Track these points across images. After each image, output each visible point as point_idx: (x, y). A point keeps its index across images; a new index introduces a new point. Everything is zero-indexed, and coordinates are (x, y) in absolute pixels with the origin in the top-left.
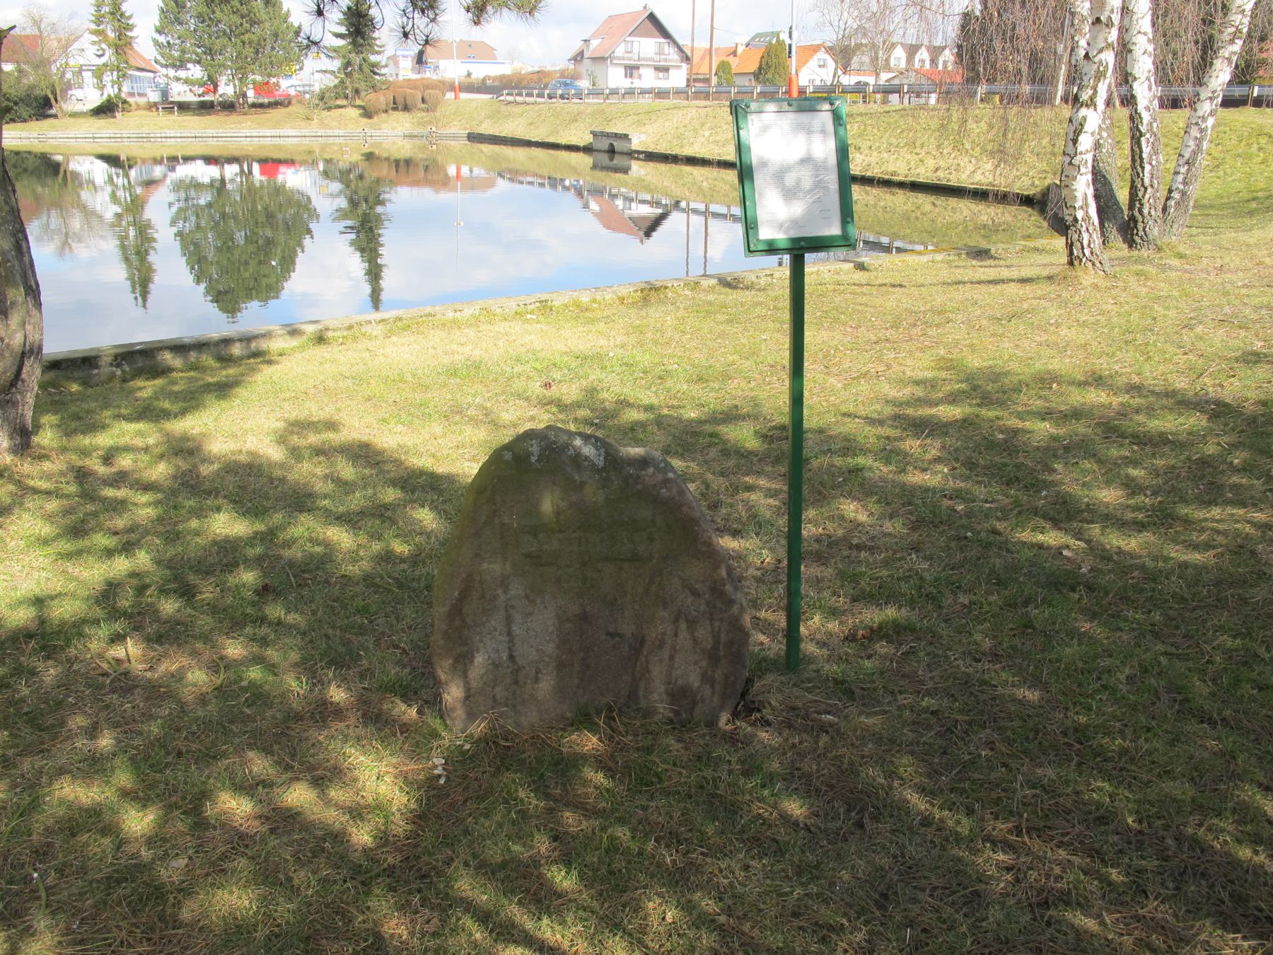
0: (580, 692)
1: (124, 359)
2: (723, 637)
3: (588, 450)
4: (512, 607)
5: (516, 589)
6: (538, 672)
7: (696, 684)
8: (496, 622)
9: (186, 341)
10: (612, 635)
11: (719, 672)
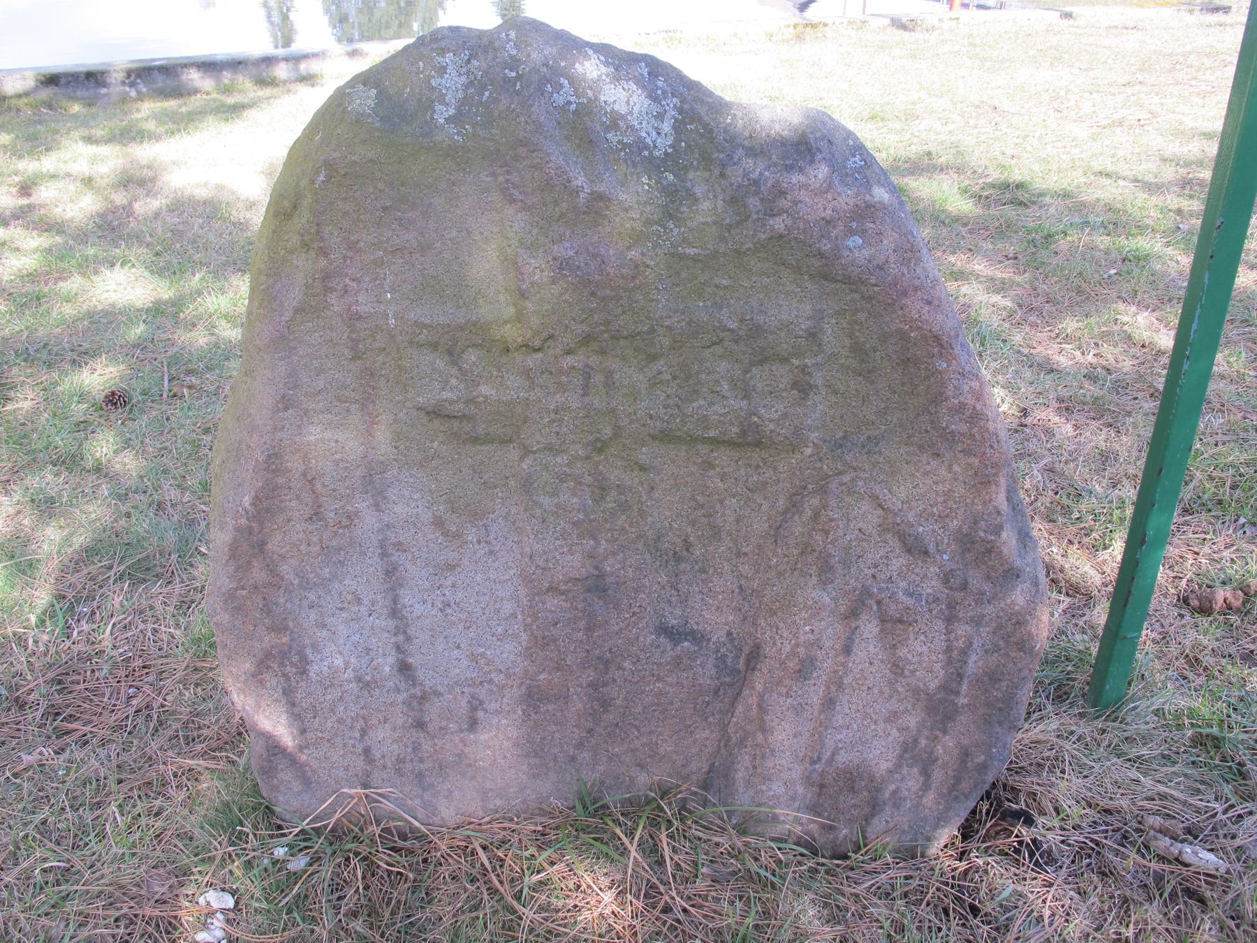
0: (586, 755)
1: (139, 76)
2: (974, 664)
3: (623, 98)
4: (399, 546)
5: (408, 504)
6: (475, 705)
7: (884, 766)
8: (362, 578)
9: (219, 58)
10: (673, 634)
11: (949, 741)
